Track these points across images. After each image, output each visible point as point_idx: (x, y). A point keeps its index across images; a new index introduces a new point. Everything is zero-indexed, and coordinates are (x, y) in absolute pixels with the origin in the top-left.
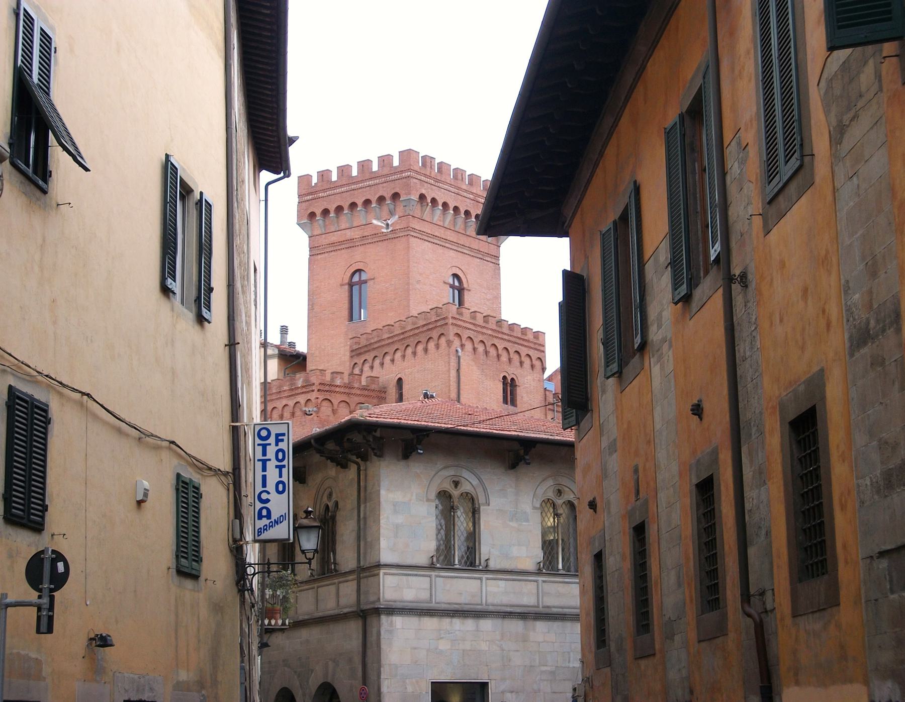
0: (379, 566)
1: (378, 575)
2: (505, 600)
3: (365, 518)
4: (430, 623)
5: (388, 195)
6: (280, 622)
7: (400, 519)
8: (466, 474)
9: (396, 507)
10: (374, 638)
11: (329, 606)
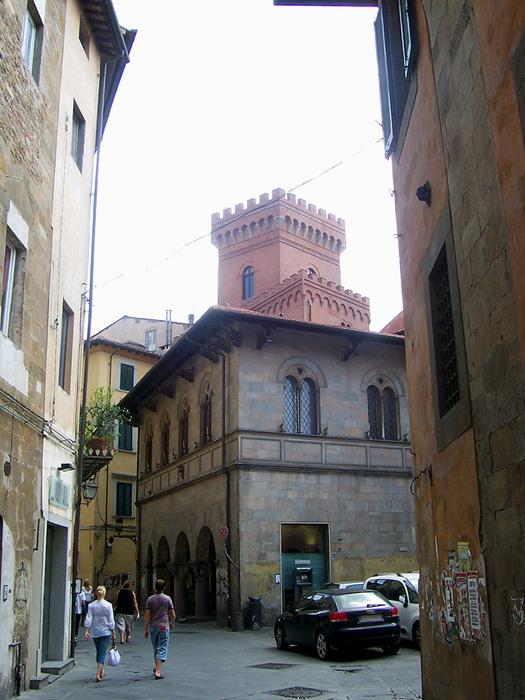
0: (238, 431)
1: (237, 439)
2: (341, 460)
3: (229, 397)
4: (280, 477)
5: (266, 218)
6: (105, 452)
7: (254, 396)
8: (307, 363)
9: (252, 387)
10: (235, 490)
11: (207, 469)
